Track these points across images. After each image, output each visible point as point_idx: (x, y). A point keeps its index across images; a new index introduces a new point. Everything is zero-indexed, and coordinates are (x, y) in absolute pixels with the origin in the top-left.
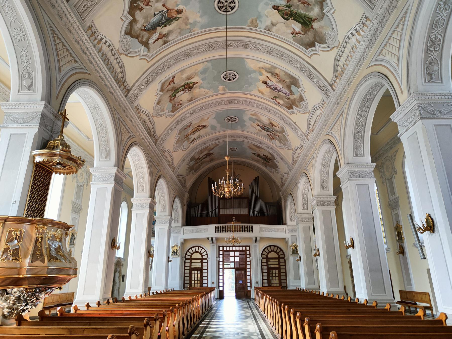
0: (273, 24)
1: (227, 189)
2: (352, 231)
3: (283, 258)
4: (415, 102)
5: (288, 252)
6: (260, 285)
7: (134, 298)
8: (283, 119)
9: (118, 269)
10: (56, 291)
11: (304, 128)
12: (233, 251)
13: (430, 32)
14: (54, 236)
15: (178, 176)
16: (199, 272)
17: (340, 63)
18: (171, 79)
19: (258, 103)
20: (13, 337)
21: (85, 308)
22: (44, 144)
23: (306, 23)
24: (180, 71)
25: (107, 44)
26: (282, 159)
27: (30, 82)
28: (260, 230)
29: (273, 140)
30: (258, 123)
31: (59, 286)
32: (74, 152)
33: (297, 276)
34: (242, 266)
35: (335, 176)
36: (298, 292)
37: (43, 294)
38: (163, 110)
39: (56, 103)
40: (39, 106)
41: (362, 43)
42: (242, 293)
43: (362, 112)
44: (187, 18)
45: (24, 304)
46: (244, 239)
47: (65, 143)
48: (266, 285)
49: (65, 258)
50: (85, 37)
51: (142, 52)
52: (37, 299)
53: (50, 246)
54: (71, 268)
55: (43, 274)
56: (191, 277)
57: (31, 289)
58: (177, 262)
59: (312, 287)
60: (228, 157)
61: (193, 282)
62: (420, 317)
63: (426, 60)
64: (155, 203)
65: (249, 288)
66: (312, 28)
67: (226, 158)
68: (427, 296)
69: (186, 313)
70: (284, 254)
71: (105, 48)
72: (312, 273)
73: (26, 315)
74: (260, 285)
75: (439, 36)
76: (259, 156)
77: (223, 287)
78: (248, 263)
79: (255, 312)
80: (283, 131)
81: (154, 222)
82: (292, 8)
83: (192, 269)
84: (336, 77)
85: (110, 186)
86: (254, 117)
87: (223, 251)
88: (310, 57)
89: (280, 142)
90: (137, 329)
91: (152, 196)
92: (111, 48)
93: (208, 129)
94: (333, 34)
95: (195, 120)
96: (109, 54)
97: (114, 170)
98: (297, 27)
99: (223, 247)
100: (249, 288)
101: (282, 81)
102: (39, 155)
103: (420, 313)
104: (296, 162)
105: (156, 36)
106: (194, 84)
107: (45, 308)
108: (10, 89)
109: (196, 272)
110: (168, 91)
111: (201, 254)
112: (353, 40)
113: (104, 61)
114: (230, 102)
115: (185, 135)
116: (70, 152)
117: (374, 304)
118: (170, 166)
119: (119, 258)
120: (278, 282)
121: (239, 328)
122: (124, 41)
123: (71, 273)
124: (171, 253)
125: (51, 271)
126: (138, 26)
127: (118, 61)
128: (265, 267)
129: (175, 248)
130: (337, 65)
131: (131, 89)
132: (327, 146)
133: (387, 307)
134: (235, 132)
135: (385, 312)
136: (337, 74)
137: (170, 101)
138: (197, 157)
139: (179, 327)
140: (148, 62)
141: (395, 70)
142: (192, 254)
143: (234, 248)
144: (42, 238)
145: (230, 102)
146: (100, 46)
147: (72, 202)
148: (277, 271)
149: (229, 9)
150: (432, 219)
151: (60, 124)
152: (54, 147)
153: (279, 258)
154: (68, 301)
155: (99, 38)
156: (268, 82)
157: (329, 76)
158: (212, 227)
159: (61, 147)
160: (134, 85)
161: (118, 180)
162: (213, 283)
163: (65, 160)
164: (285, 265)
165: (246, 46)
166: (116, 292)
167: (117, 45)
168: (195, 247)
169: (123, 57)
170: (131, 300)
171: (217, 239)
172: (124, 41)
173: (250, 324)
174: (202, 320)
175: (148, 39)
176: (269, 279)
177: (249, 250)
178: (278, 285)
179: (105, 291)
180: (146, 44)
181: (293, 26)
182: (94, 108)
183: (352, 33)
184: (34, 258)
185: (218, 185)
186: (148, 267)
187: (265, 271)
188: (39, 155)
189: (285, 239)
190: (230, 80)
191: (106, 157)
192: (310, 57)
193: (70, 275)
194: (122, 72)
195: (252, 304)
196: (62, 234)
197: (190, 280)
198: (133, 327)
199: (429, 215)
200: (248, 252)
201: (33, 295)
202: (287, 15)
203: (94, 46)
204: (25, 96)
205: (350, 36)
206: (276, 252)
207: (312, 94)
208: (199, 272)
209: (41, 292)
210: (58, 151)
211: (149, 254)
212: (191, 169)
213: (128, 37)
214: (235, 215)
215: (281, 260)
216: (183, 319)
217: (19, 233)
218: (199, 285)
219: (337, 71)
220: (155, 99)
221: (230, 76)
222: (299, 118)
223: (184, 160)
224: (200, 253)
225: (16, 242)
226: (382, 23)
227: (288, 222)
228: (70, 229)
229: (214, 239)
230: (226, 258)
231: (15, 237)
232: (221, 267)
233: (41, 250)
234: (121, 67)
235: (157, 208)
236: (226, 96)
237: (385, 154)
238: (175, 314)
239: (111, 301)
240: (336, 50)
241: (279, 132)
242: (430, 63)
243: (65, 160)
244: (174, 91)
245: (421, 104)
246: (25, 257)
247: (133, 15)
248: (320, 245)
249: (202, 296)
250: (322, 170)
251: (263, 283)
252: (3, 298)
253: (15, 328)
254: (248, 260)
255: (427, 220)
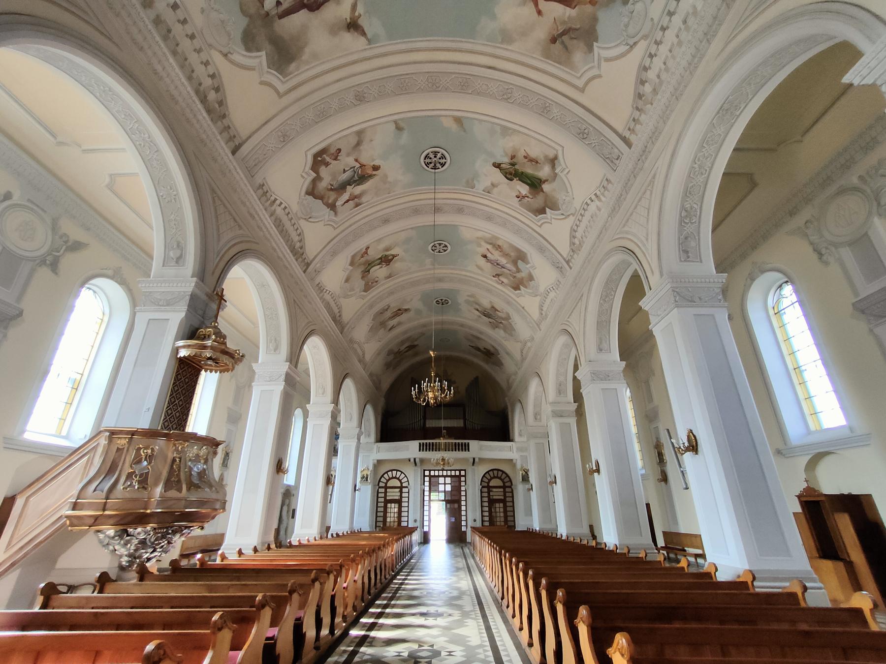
0: (493, 185)
1: (432, 392)
2: (598, 452)
3: (510, 487)
4: (669, 286)
5: (517, 479)
6: (478, 524)
7: (305, 542)
8: (508, 303)
9: (287, 501)
10: (196, 532)
11: (536, 315)
12: (443, 476)
13: (684, 200)
14: (197, 456)
15: (371, 375)
16: (397, 505)
17: (578, 235)
18: (364, 250)
19: (476, 283)
20: (128, 597)
21: (236, 557)
22: (192, 333)
23: (535, 184)
24: (375, 241)
25: (283, 206)
26: (508, 354)
27: (178, 253)
28: (481, 449)
29: (497, 329)
30: (477, 307)
31: (200, 524)
32: (231, 345)
33: (529, 512)
34: (454, 498)
35: (575, 378)
36: (529, 534)
37: (178, 535)
38: (352, 289)
39: (211, 280)
40: (188, 284)
41: (603, 210)
42: (456, 537)
43: (606, 296)
44: (386, 176)
45: (151, 550)
46: (457, 460)
47: (220, 332)
48: (487, 524)
49: (210, 486)
50: (253, 197)
51: (327, 217)
52: (169, 543)
53: (191, 469)
54: (218, 500)
55: (178, 508)
56: (385, 512)
57: (160, 528)
58: (366, 493)
59: (547, 527)
60: (433, 351)
61: (388, 520)
62: (683, 568)
63: (680, 231)
64: (339, 411)
65: (464, 529)
66: (542, 191)
67: (431, 353)
68: (698, 539)
69: (374, 564)
70: (510, 481)
71: (279, 211)
72: (547, 507)
73: (151, 566)
74: (478, 524)
75: (695, 206)
76: (478, 349)
77: (429, 526)
78: (463, 493)
79: (471, 561)
80: (508, 318)
81: (337, 437)
82: (517, 167)
83: (387, 502)
84: (573, 251)
85: (279, 387)
86: (472, 299)
87: (430, 476)
88: (540, 226)
89: (505, 331)
90: (302, 586)
91: (336, 401)
92: (287, 211)
93: (411, 314)
94: (568, 199)
95: (394, 302)
96: (285, 219)
97: (285, 367)
98: (524, 189)
99: (430, 471)
100: (464, 529)
101: (506, 255)
102: (184, 347)
103: (683, 563)
104: (581, 245)
105: (346, 196)
106: (394, 256)
107: (183, 556)
108: (152, 259)
109: (393, 505)
110: (360, 265)
111: (400, 481)
112: (593, 207)
113: (277, 227)
114: (440, 280)
115: (381, 322)
116: (225, 344)
117: (626, 551)
118: (360, 361)
119: (289, 486)
120: (503, 519)
121: (447, 585)
122: (305, 202)
123: (218, 506)
124: (359, 479)
125: (191, 504)
126: (323, 185)
127: (298, 232)
128: (486, 499)
129: (365, 473)
130: (574, 237)
131: (311, 262)
132: (563, 339)
133: (642, 555)
134: (445, 318)
135: (638, 561)
136: (574, 248)
137: (363, 278)
138: (396, 350)
139: (363, 583)
140: (335, 229)
141: (644, 245)
142: (388, 481)
143: (445, 473)
144: (180, 458)
145: (440, 280)
146: (273, 208)
147: (229, 408)
148: (502, 505)
149: (438, 165)
150: (694, 436)
151: (215, 307)
152: (205, 337)
153: (504, 487)
154: (212, 546)
155: (272, 198)
156: (489, 255)
157: (565, 250)
158: (414, 444)
159: (213, 337)
160: (316, 257)
161: (290, 380)
162: (415, 521)
163: (218, 354)
164: (513, 497)
165: (460, 210)
166: (282, 532)
167: (295, 207)
168: (392, 471)
169: (302, 223)
170: (301, 545)
171: (422, 461)
172: (305, 202)
173: (462, 579)
174: (398, 574)
175: (336, 200)
176: (490, 516)
177: (465, 476)
178: (503, 524)
179: (265, 532)
180: (332, 207)
181: (518, 187)
182: (262, 286)
183: (590, 199)
184: (168, 486)
185: (420, 388)
186: (326, 499)
187: (486, 504)
188: (184, 347)
189: (512, 460)
190: (439, 252)
191: (275, 350)
192: (540, 226)
193: (216, 510)
194: (300, 241)
195: (467, 551)
196: (209, 452)
197: (385, 517)
198: (294, 583)
199: (691, 431)
200: (463, 479)
201: (163, 537)
202: (511, 174)
203: (266, 210)
204: (171, 271)
205: (589, 202)
206: (500, 478)
207: (543, 272)
208: (397, 505)
209: (174, 533)
210: (209, 343)
211: (329, 480)
212: (388, 366)
213: (310, 198)
214: (445, 428)
215: (508, 490)
216: (369, 571)
217: (149, 451)
218: (396, 524)
219: (574, 244)
220: (342, 275)
221: (440, 247)
222: (528, 301)
223: (379, 354)
224: (398, 479)
225: (145, 463)
226: (626, 187)
227: (517, 437)
228: (220, 447)
229: (417, 460)
230: (433, 486)
231: (144, 457)
232: (426, 498)
233: (178, 475)
234: (299, 235)
235: (342, 418)
236: (432, 272)
237: (636, 350)
238: (357, 565)
239: (273, 546)
240: (572, 218)
241: (503, 319)
242: (686, 238)
243: (218, 354)
244: (367, 265)
245: (677, 288)
246: (156, 484)
247: (317, 172)
248: (557, 468)
249: (397, 540)
250: (558, 370)
251: (483, 521)
252: (122, 542)
253: (134, 584)
254: (463, 488)
255: (688, 437)
